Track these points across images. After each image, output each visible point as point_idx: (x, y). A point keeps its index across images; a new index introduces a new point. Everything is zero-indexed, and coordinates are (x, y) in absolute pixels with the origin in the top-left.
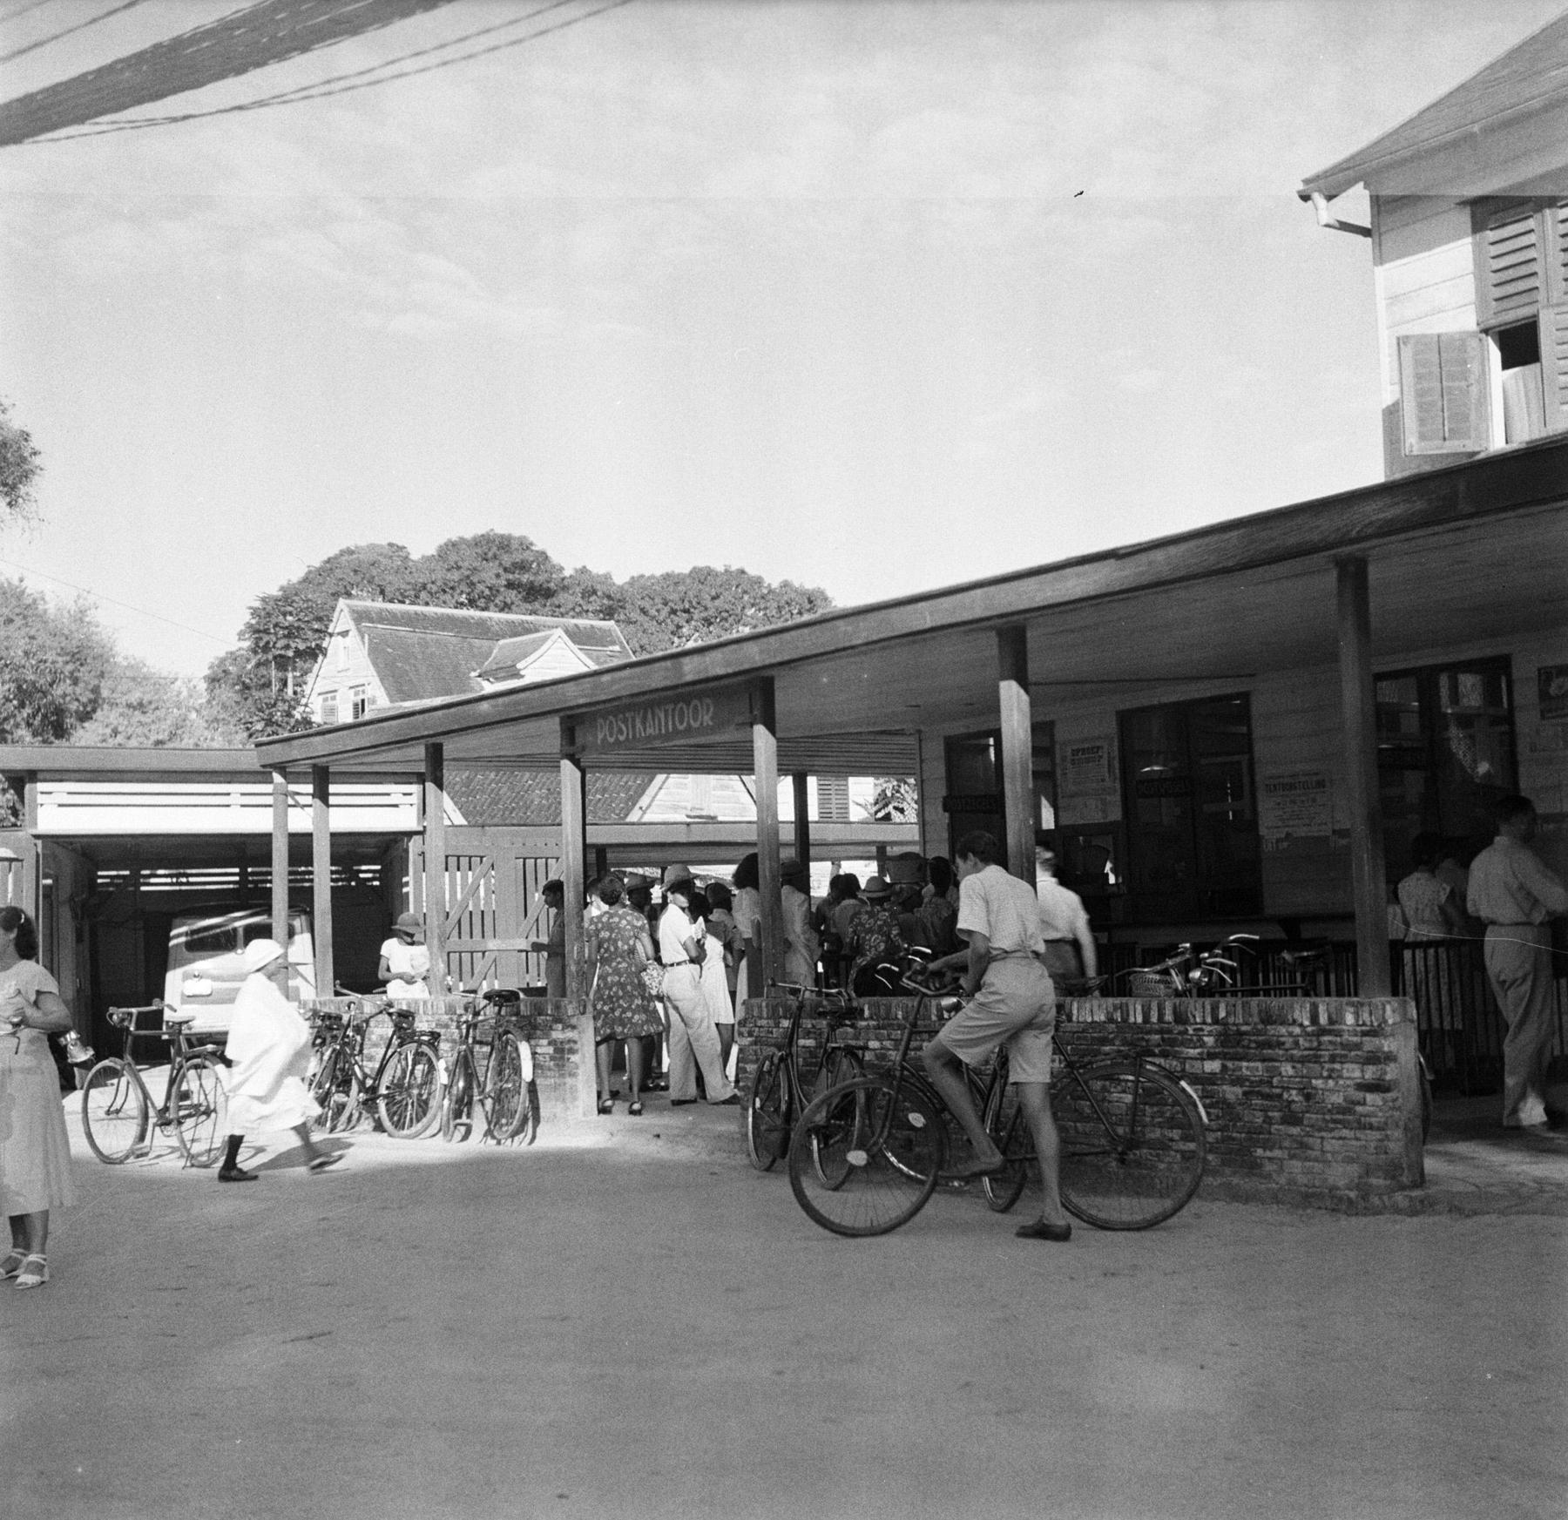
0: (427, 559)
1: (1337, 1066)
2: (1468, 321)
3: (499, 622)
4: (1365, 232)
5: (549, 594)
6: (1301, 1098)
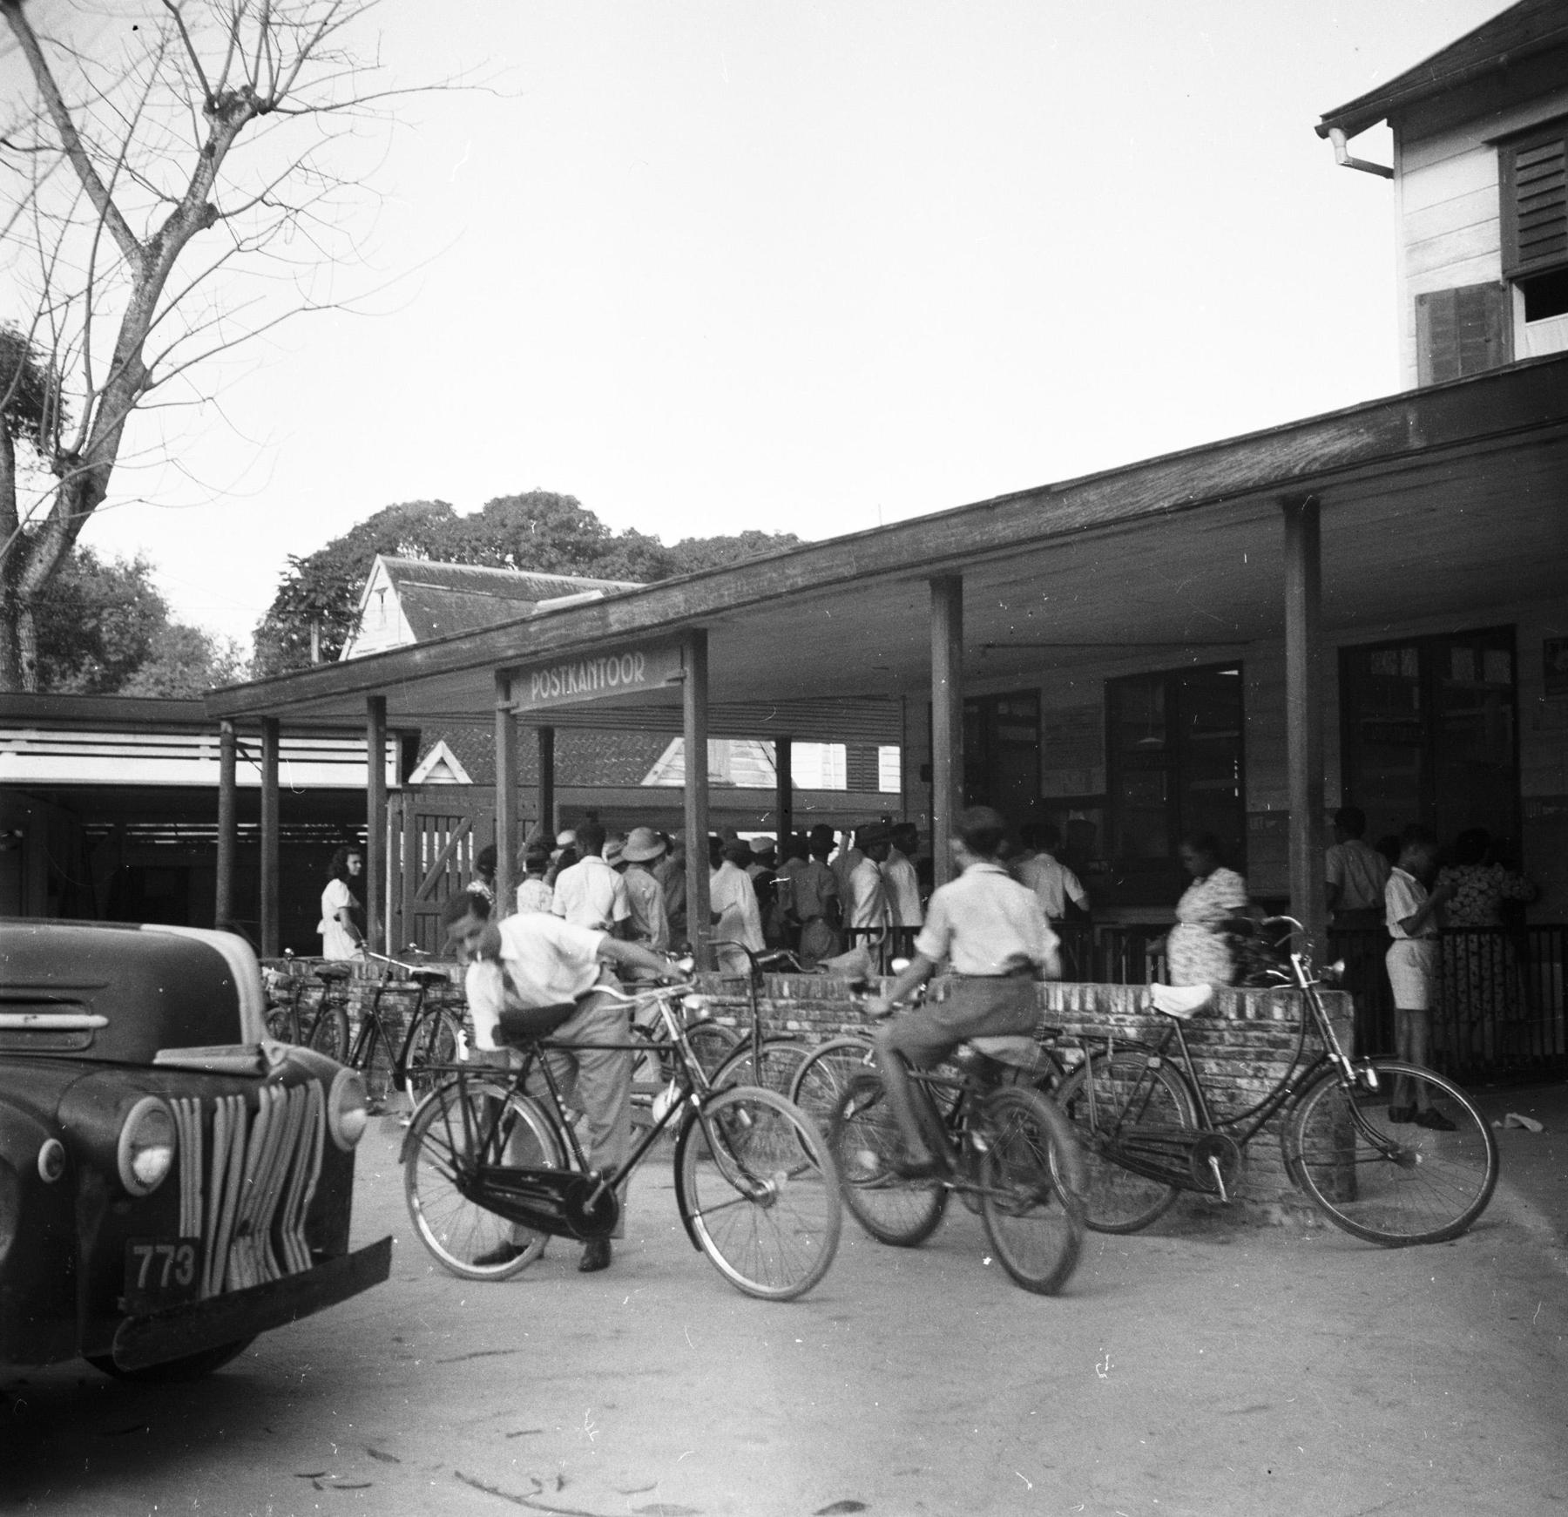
0: (473, 517)
1: (1263, 1064)
2: (1491, 271)
3: (539, 583)
4: (1387, 173)
5: (596, 555)
6: (1223, 1099)
